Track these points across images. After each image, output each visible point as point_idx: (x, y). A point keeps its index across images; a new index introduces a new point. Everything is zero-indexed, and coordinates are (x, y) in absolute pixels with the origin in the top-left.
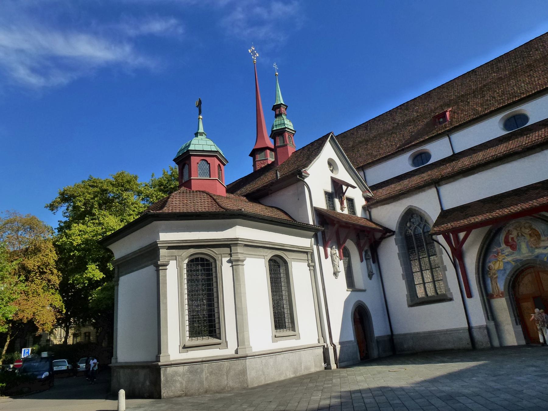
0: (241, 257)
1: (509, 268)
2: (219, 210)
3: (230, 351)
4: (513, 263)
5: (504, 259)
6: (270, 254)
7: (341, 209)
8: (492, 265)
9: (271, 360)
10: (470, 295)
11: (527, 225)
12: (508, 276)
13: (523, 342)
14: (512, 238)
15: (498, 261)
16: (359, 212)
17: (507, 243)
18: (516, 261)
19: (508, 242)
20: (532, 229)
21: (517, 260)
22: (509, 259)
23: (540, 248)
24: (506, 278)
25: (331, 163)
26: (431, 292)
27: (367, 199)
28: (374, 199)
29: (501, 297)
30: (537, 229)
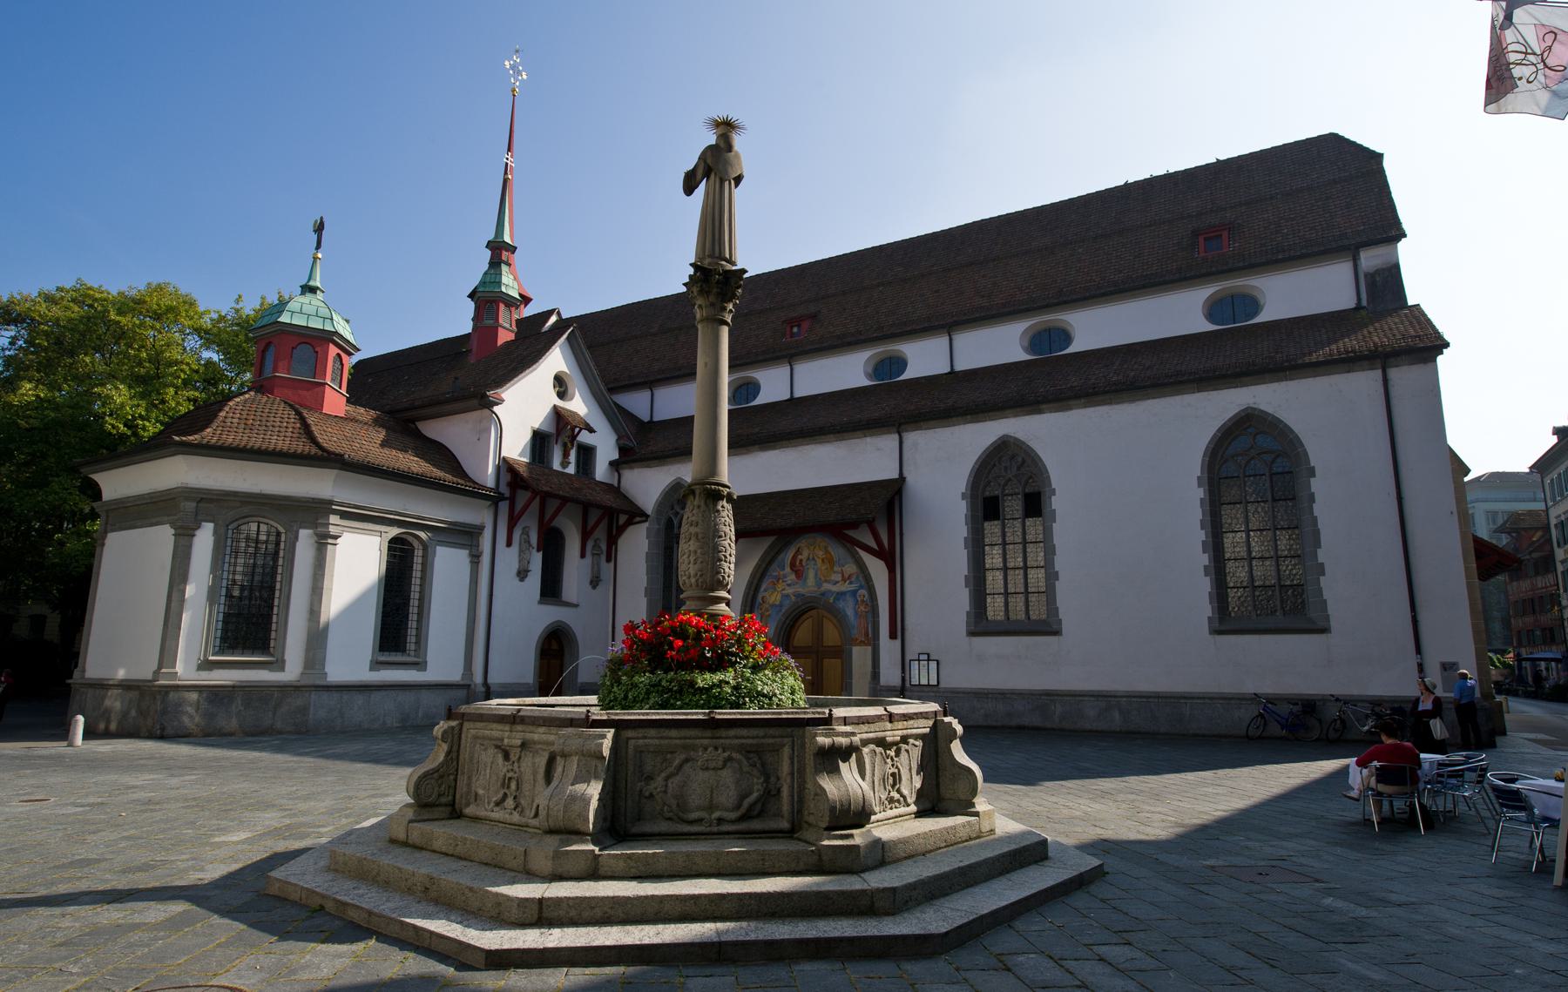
0: (333, 530)
1: (787, 603)
2: (314, 450)
3: (292, 671)
6: (394, 531)
7: (562, 463)
9: (359, 699)
16: (601, 471)
18: (797, 595)
25: (560, 381)
26: (1018, 612)
27: (623, 450)
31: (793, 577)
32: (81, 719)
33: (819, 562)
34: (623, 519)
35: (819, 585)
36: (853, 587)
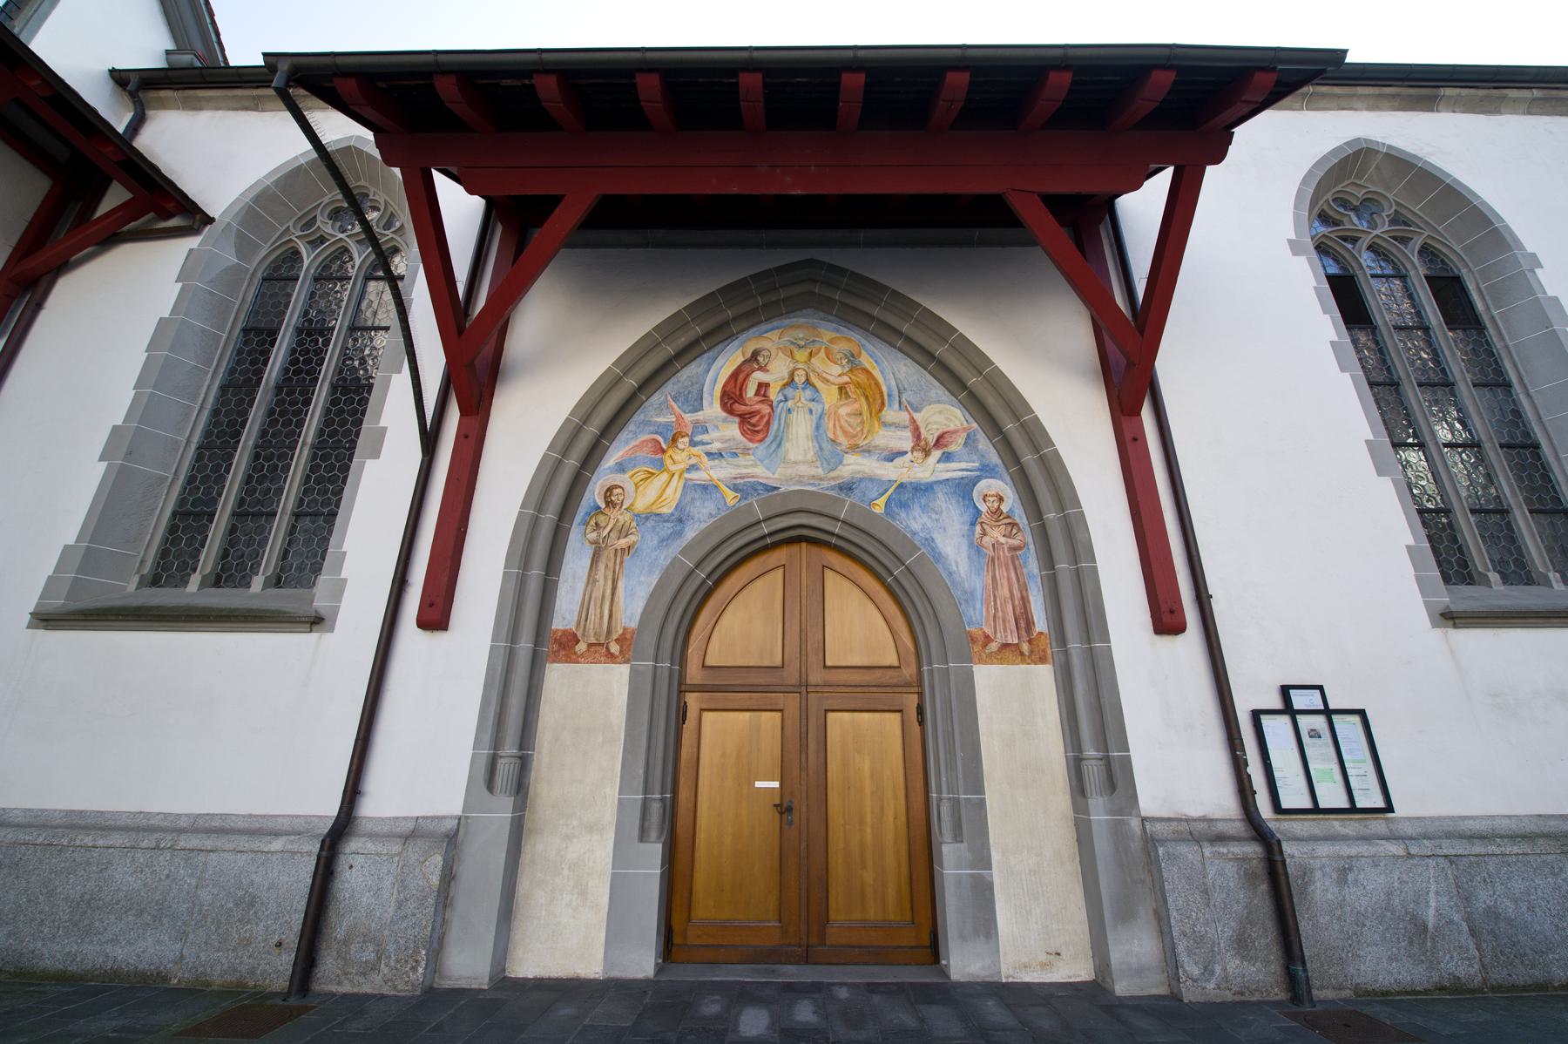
1: (704, 514)
4: (730, 495)
5: (693, 468)
8: (629, 487)
10: (436, 617)
12: (684, 552)
13: (642, 963)
14: (763, 387)
17: (731, 398)
29: (611, 658)
30: (877, 373)
31: (732, 430)
32: (758, 784)
33: (829, 395)
34: (115, 197)
35: (834, 461)
36: (953, 470)
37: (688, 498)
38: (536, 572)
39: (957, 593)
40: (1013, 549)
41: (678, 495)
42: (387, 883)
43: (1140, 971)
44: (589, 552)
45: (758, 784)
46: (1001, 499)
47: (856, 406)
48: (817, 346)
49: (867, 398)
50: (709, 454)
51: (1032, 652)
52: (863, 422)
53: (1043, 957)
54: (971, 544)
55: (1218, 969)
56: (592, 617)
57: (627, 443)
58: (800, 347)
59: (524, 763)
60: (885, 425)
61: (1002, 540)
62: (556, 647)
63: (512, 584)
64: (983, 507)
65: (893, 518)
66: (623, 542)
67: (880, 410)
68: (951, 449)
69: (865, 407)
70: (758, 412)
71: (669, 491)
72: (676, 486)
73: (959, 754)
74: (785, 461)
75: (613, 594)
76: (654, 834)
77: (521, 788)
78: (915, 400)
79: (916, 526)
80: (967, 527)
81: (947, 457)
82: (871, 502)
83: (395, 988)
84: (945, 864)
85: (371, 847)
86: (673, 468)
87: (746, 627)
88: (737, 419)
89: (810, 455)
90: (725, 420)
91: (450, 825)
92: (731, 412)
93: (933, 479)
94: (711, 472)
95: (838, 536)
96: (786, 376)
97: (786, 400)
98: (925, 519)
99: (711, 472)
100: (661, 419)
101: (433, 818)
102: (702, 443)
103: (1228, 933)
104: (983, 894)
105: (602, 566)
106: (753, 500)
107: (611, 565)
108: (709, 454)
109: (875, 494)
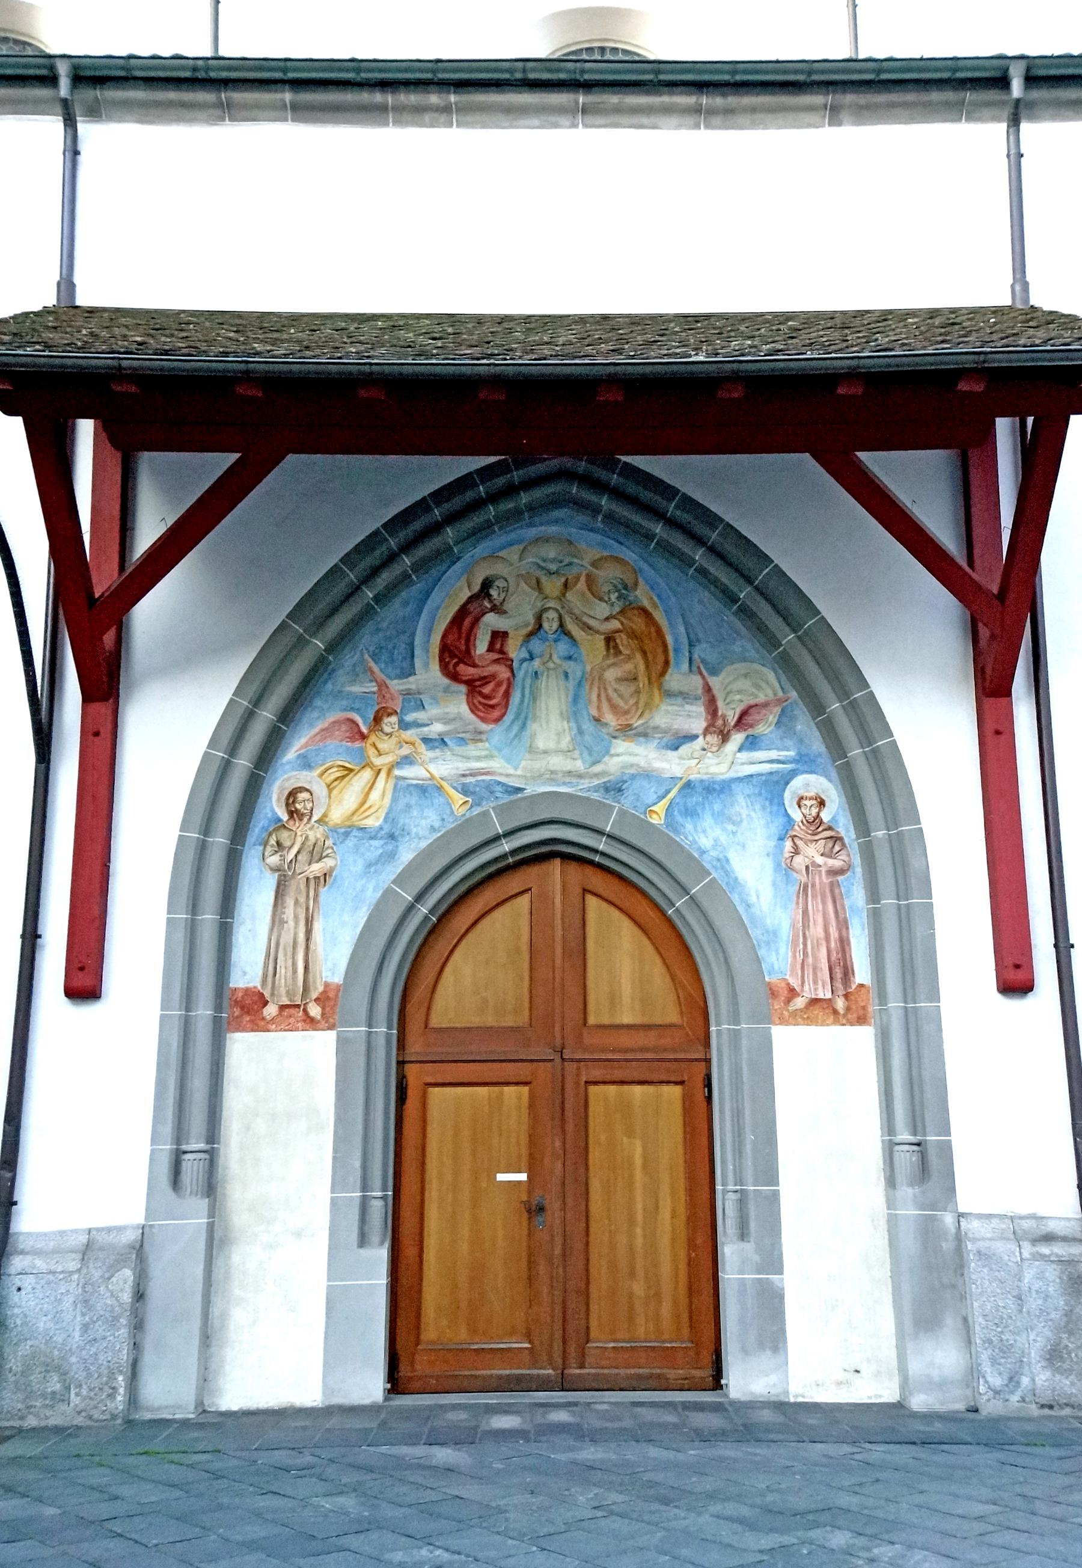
1: (424, 827)
4: (458, 798)
5: (407, 760)
8: (319, 789)
10: (84, 985)
11: (609, 574)
12: (399, 880)
13: (369, 1385)
14: (498, 637)
15: (368, 765)
17: (454, 656)
19: (466, 656)
20: (630, 608)
21: (489, 787)
22: (442, 766)
23: (644, 735)
24: (388, 893)
28: (837, 813)
29: (310, 1023)
30: (659, 616)
31: (459, 706)
32: (501, 1177)
37: (401, 804)
38: (209, 917)
39: (755, 933)
40: (834, 872)
41: (387, 801)
42: (67, 1303)
43: (942, 1385)
44: (270, 882)
45: (501, 1177)
46: (822, 803)
47: (629, 666)
48: (575, 570)
49: (644, 653)
50: (426, 740)
51: (848, 1009)
52: (638, 692)
53: (841, 1376)
54: (777, 867)
55: (1025, 1381)
56: (281, 971)
57: (312, 725)
58: (550, 573)
59: (212, 1157)
60: (669, 694)
61: (820, 860)
62: (237, 1012)
63: (180, 936)
64: (797, 815)
65: (676, 831)
66: (316, 868)
67: (663, 673)
68: (760, 729)
69: (642, 667)
70: (493, 676)
71: (375, 795)
72: (381, 795)
73: (750, 1137)
74: (531, 750)
75: (308, 939)
76: (375, 1236)
77: (211, 1187)
78: (712, 657)
79: (705, 842)
80: (773, 843)
81: (752, 743)
82: (648, 810)
83: (90, 1418)
84: (728, 1267)
85: (41, 1264)
86: (378, 761)
87: (482, 979)
88: (463, 688)
89: (565, 742)
90: (446, 690)
91: (132, 1236)
92: (455, 677)
93: (732, 774)
94: (432, 768)
95: (603, 854)
96: (532, 621)
97: (532, 658)
98: (718, 832)
99: (432, 768)
100: (356, 689)
101: (109, 1230)
102: (417, 724)
103: (1041, 1342)
104: (771, 1304)
105: (290, 902)
106: (488, 806)
107: (302, 900)
108: (426, 740)
109: (653, 797)
